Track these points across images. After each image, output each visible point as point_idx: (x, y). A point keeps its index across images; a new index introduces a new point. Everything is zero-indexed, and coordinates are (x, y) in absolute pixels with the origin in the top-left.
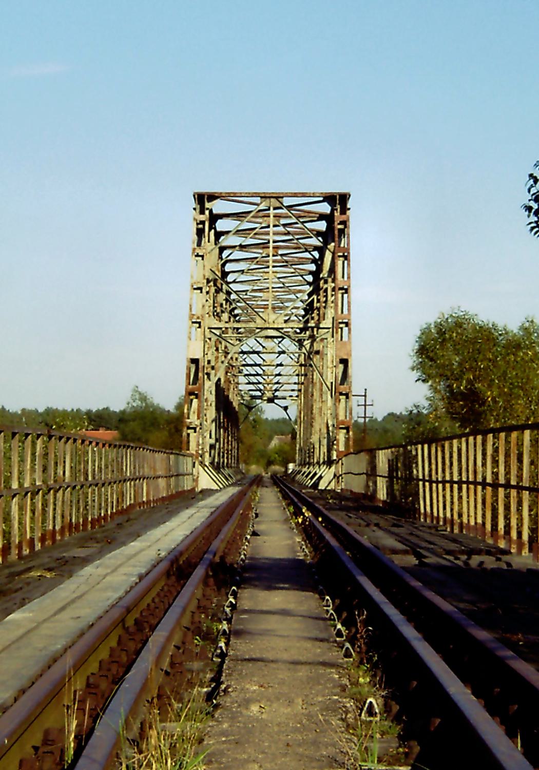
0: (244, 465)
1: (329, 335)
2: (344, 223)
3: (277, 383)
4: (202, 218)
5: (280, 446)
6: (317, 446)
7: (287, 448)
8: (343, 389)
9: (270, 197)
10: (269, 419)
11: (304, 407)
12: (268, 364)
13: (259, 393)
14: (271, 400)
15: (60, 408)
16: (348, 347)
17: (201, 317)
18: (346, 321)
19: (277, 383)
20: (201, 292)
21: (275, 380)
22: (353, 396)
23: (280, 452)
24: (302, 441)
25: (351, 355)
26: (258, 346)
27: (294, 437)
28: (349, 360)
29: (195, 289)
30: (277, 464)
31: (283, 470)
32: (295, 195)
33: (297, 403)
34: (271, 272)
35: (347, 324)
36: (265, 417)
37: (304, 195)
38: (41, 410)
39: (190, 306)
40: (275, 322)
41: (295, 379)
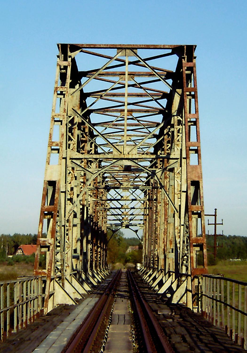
0: (111, 264)
1: (178, 164)
2: (191, 69)
3: (132, 214)
4: (65, 63)
5: (132, 252)
6: (162, 257)
7: (136, 254)
8: (195, 208)
9: (125, 49)
10: (127, 238)
11: (149, 230)
12: (124, 199)
13: (119, 222)
14: (127, 227)
15: (21, 234)
16: (199, 170)
17: (60, 145)
18: (196, 148)
19: (132, 214)
20: (61, 124)
21: (130, 213)
22: (205, 215)
23: (132, 255)
24: (147, 252)
25: (202, 177)
26: (119, 191)
27: (141, 247)
28: (200, 182)
29: (55, 121)
30: (131, 262)
31: (134, 266)
32: (148, 47)
33: (143, 228)
34: (125, 136)
35: (197, 151)
36: (124, 237)
37: (155, 47)
38: (12, 235)
39: (50, 134)
40: (130, 153)
41: (142, 217)
